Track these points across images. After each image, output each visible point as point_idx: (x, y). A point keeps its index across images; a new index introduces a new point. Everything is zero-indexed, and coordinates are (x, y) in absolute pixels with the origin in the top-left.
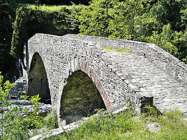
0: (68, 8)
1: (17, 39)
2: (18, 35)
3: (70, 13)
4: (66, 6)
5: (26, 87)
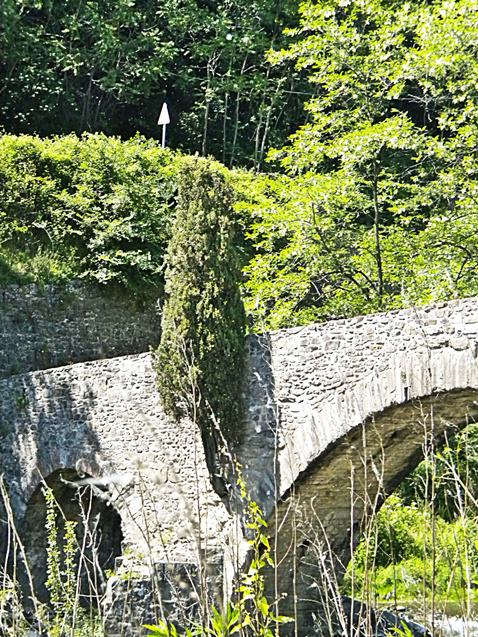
0: (57, 148)
1: (210, 322)
2: (214, 302)
3: (66, 184)
4: (37, 140)
5: (220, 585)
